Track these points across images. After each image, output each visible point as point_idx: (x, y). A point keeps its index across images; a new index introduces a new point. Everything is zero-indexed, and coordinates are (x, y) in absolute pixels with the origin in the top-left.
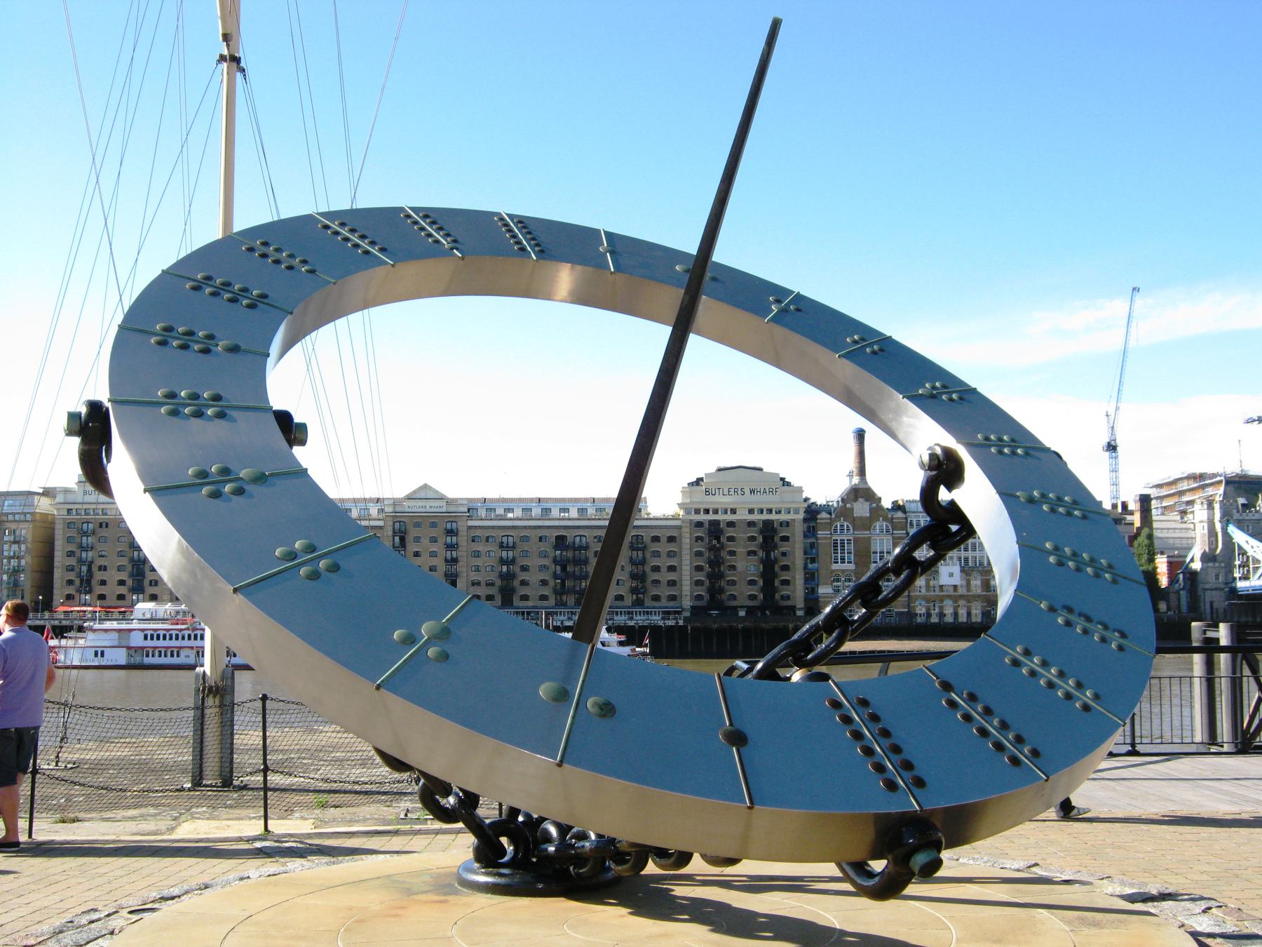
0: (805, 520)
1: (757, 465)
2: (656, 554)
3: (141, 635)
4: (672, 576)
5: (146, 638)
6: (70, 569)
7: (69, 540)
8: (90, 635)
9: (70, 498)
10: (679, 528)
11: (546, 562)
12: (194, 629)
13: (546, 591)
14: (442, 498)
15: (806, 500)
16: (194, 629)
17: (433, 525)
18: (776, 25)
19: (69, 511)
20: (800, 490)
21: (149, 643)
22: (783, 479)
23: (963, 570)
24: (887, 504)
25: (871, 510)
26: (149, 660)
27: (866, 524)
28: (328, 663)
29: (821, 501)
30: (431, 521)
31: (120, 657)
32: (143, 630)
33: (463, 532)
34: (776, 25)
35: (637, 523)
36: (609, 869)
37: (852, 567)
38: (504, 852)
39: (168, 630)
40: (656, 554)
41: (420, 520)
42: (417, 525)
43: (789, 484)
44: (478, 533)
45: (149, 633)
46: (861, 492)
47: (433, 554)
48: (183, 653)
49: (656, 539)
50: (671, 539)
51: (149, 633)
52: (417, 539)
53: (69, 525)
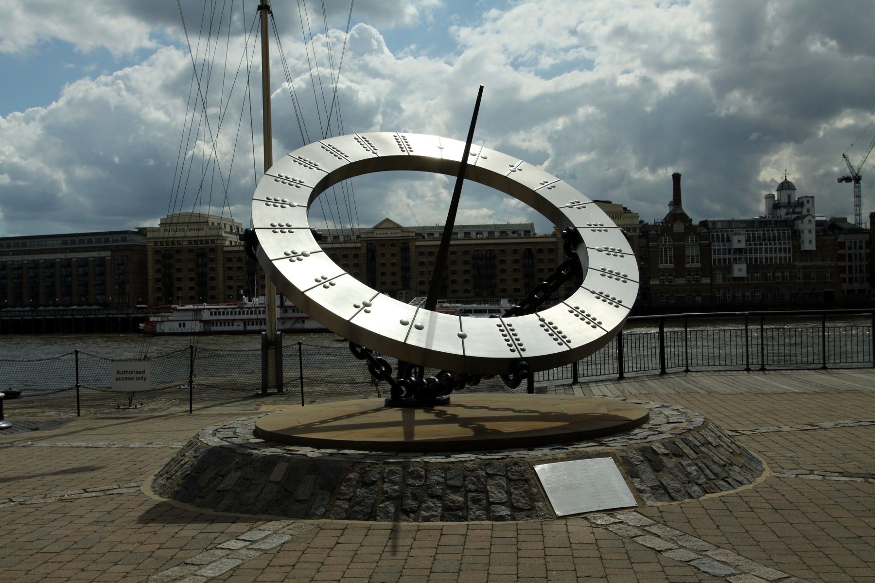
0: (640, 237)
1: (608, 199)
2: (541, 261)
3: (208, 312)
4: (231, 283)
5: (211, 314)
6: (158, 280)
7: (157, 262)
8: (175, 313)
9: (156, 235)
10: (556, 243)
11: (468, 267)
12: (242, 308)
13: (469, 287)
14: (398, 227)
15: (641, 222)
16: (242, 308)
17: (393, 245)
18: (481, 88)
19: (155, 242)
20: (637, 216)
21: (214, 317)
22: (625, 209)
23: (748, 267)
24: (696, 221)
25: (685, 227)
26: (214, 328)
27: (681, 237)
28: (286, 427)
29: (651, 222)
30: (392, 242)
31: (198, 327)
32: (209, 309)
33: (413, 249)
34: (481, 88)
35: (452, 242)
36: (437, 376)
37: (672, 266)
38: (403, 392)
39: (225, 309)
40: (541, 261)
41: (383, 243)
42: (383, 245)
43: (629, 212)
44: (423, 250)
45: (213, 311)
46: (677, 214)
47: (394, 264)
48: (235, 324)
49: (540, 251)
50: (551, 251)
51: (213, 311)
52: (383, 255)
53: (157, 252)
